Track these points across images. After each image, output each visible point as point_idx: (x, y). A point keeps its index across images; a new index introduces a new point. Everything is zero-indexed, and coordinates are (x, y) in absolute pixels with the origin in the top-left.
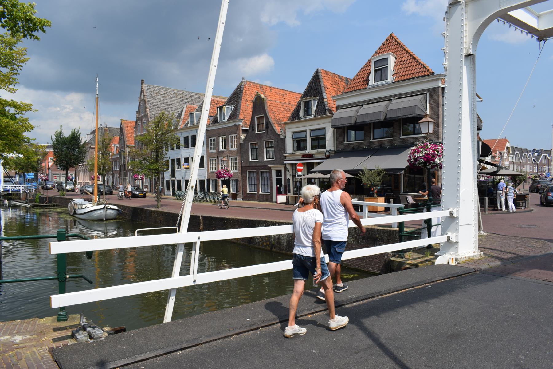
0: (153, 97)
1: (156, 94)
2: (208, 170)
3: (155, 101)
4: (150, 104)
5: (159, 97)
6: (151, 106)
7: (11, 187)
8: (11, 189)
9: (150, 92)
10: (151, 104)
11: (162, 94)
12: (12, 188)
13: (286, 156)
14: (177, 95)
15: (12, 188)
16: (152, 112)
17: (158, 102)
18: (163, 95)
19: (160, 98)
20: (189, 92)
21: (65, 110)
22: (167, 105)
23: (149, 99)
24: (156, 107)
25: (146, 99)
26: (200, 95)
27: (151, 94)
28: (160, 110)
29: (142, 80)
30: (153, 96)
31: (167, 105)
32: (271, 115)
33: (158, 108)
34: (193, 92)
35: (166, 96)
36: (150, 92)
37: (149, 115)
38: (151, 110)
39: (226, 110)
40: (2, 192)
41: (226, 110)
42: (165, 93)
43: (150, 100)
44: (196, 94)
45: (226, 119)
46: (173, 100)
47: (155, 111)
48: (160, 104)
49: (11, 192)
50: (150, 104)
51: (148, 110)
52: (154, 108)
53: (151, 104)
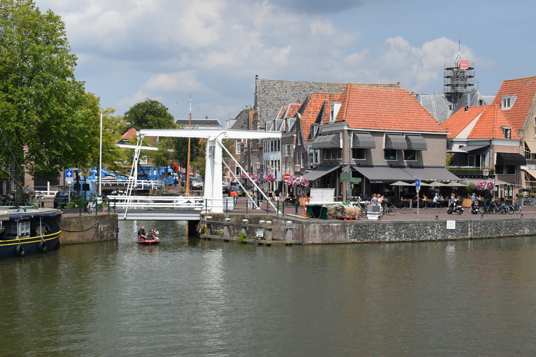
0: (266, 93)
1: (269, 90)
2: (282, 173)
3: (267, 97)
4: (261, 101)
5: (272, 92)
6: (263, 103)
7: (144, 182)
8: (144, 185)
9: (264, 88)
10: (263, 101)
11: (276, 88)
12: (145, 184)
13: (307, 166)
14: (293, 88)
15: (145, 184)
16: (263, 110)
17: (271, 98)
18: (278, 90)
19: (273, 93)
20: (309, 82)
21: (113, 192)
22: (280, 100)
23: (261, 96)
24: (268, 103)
25: (258, 96)
26: (322, 84)
27: (265, 89)
28: (271, 106)
29: (257, 76)
30: (266, 91)
31: (280, 100)
32: (306, 132)
33: (270, 105)
34: (313, 83)
35: (281, 90)
36: (264, 88)
37: (259, 113)
38: (261, 108)
39: (289, 122)
40: (136, 187)
41: (289, 122)
42: (280, 87)
43: (262, 96)
44: (317, 84)
45: (289, 130)
46: (288, 94)
47: (267, 108)
48: (272, 100)
49: (144, 188)
50: (261, 101)
51: (258, 108)
52: (266, 105)
53: (263, 101)
